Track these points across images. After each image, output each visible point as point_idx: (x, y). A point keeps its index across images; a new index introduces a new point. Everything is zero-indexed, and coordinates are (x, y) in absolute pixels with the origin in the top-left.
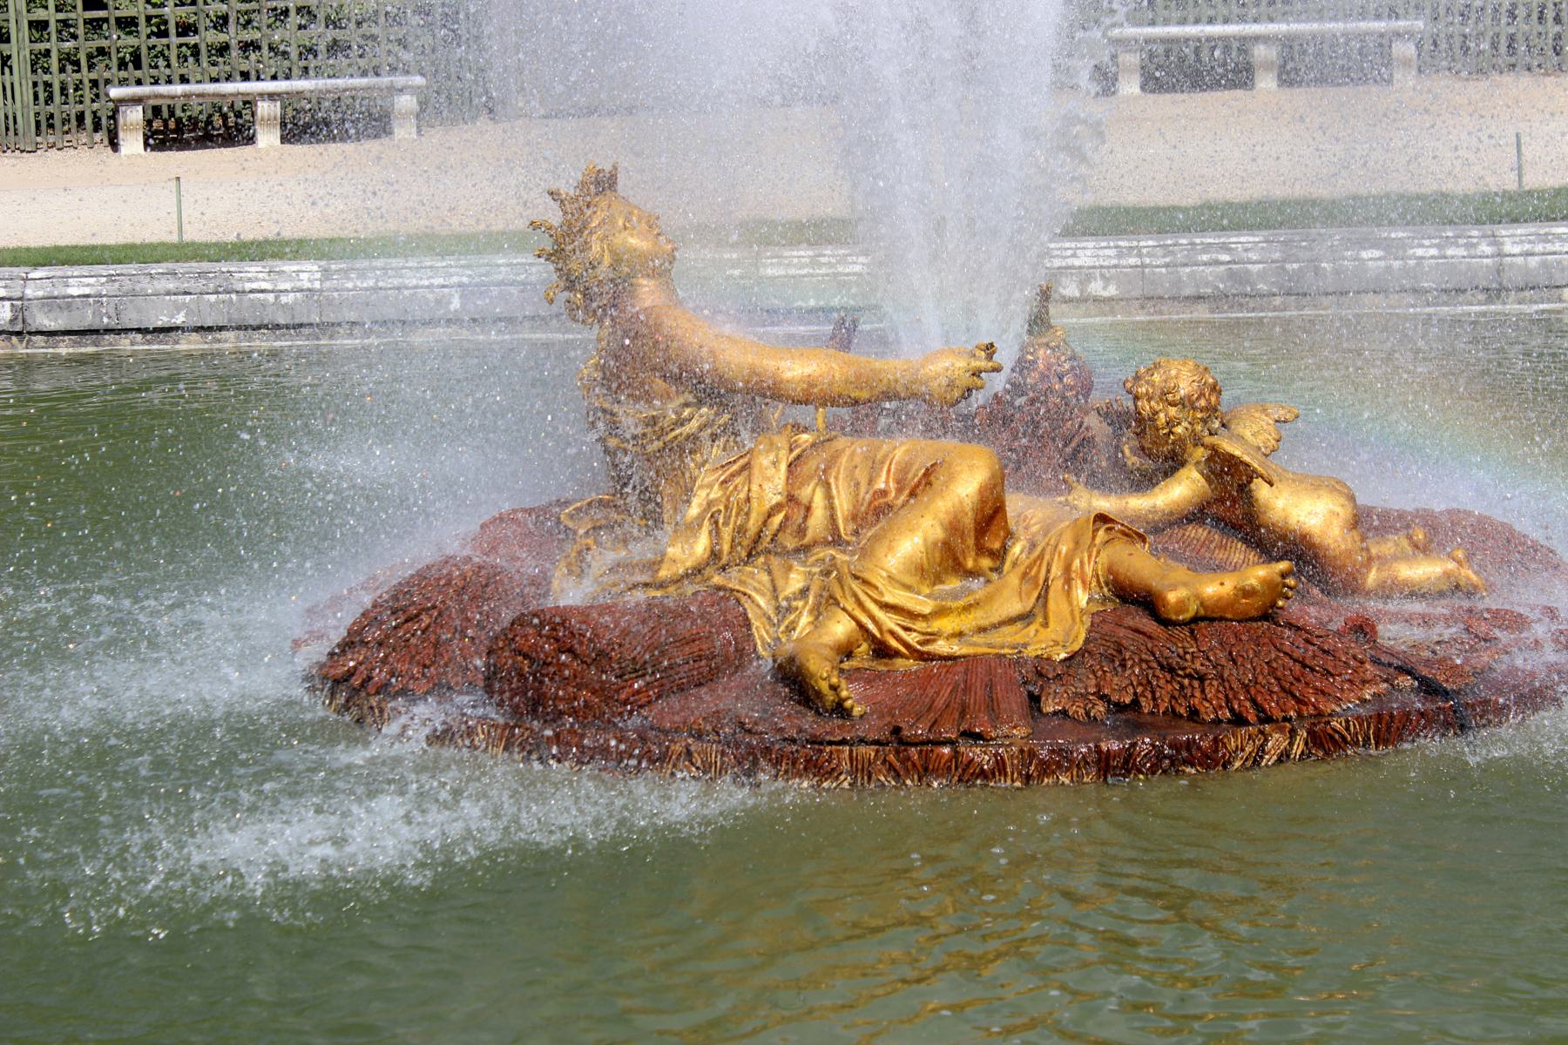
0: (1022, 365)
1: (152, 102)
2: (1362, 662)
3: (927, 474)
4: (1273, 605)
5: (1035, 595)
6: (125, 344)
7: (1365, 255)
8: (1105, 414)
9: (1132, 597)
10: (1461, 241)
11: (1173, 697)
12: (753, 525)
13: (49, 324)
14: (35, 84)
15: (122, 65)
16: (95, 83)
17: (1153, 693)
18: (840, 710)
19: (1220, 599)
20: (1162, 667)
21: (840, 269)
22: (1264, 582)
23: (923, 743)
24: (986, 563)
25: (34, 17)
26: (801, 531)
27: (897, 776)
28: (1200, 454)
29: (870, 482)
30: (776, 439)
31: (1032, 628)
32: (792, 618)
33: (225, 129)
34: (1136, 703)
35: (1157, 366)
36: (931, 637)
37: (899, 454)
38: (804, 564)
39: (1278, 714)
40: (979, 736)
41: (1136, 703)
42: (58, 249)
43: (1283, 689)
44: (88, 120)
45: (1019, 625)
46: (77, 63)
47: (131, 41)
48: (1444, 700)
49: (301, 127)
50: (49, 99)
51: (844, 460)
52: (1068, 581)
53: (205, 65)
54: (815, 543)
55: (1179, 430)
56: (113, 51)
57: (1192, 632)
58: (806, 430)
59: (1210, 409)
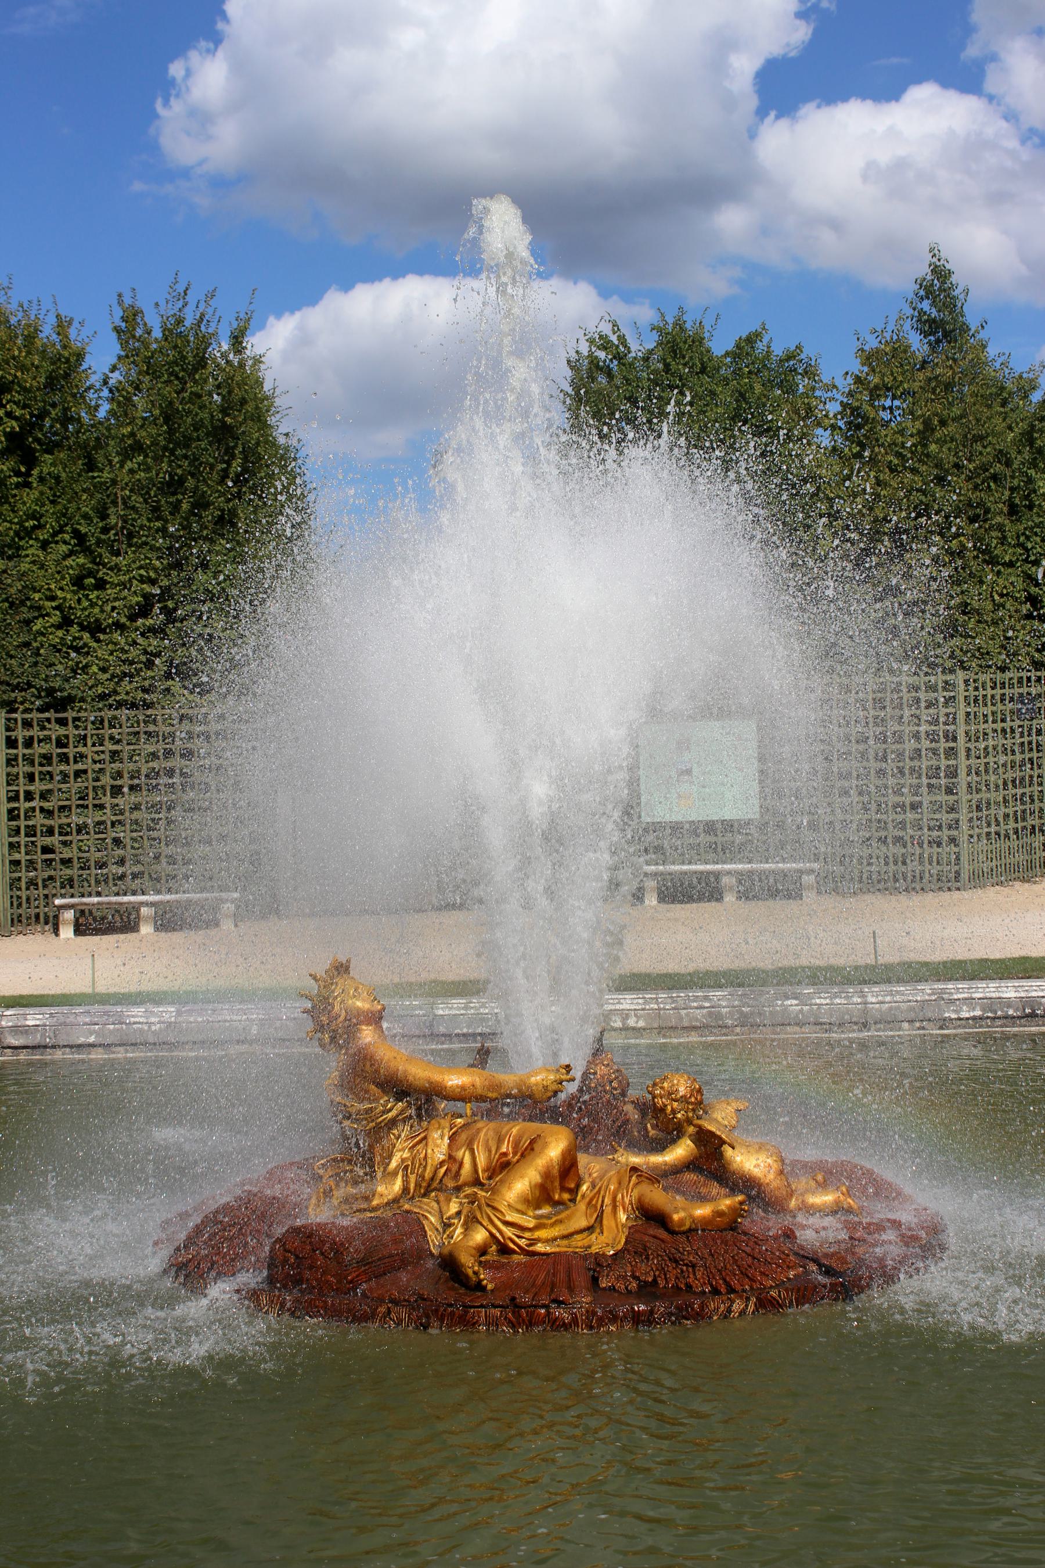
0: (585, 1075)
1: (79, 907)
2: (788, 1255)
3: (532, 1142)
4: (736, 1221)
5: (595, 1215)
6: (58, 1054)
7: (789, 1002)
8: (635, 1104)
9: (652, 1217)
10: (843, 995)
11: (677, 1278)
12: (428, 1175)
13: (15, 1042)
14: (12, 897)
15: (63, 887)
16: (46, 896)
17: (665, 1275)
18: (480, 1287)
19: (704, 1218)
20: (670, 1259)
21: (482, 1010)
22: (729, 1207)
23: (529, 1307)
24: (566, 1196)
25: (12, 858)
26: (458, 1174)
27: (513, 1327)
28: (691, 1129)
29: (498, 1148)
30: (442, 1121)
31: (594, 1236)
32: (451, 1229)
33: (124, 923)
34: (655, 1280)
35: (665, 1078)
36: (533, 1242)
37: (515, 1131)
38: (457, 1197)
39: (738, 1288)
40: (562, 1302)
41: (655, 1280)
42: (21, 997)
43: (742, 1273)
44: (42, 919)
45: (586, 1234)
46: (37, 884)
47: (68, 872)
48: (840, 1278)
49: (168, 921)
50: (20, 905)
51: (482, 1135)
52: (615, 1208)
53: (111, 885)
54: (465, 1184)
55: (679, 1116)
56: (58, 878)
57: (688, 1237)
58: (461, 1116)
59: (697, 1103)
